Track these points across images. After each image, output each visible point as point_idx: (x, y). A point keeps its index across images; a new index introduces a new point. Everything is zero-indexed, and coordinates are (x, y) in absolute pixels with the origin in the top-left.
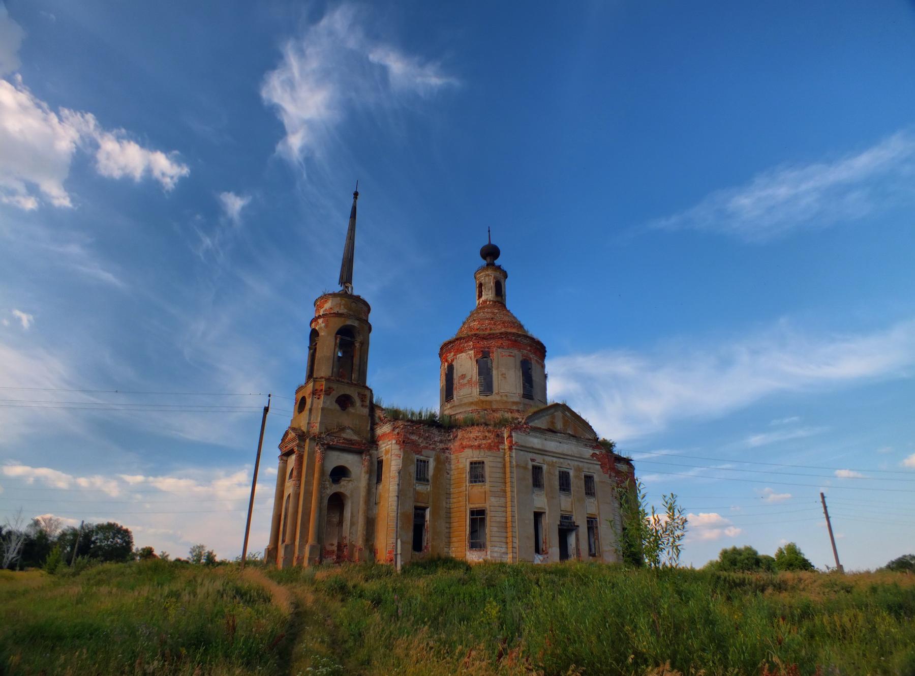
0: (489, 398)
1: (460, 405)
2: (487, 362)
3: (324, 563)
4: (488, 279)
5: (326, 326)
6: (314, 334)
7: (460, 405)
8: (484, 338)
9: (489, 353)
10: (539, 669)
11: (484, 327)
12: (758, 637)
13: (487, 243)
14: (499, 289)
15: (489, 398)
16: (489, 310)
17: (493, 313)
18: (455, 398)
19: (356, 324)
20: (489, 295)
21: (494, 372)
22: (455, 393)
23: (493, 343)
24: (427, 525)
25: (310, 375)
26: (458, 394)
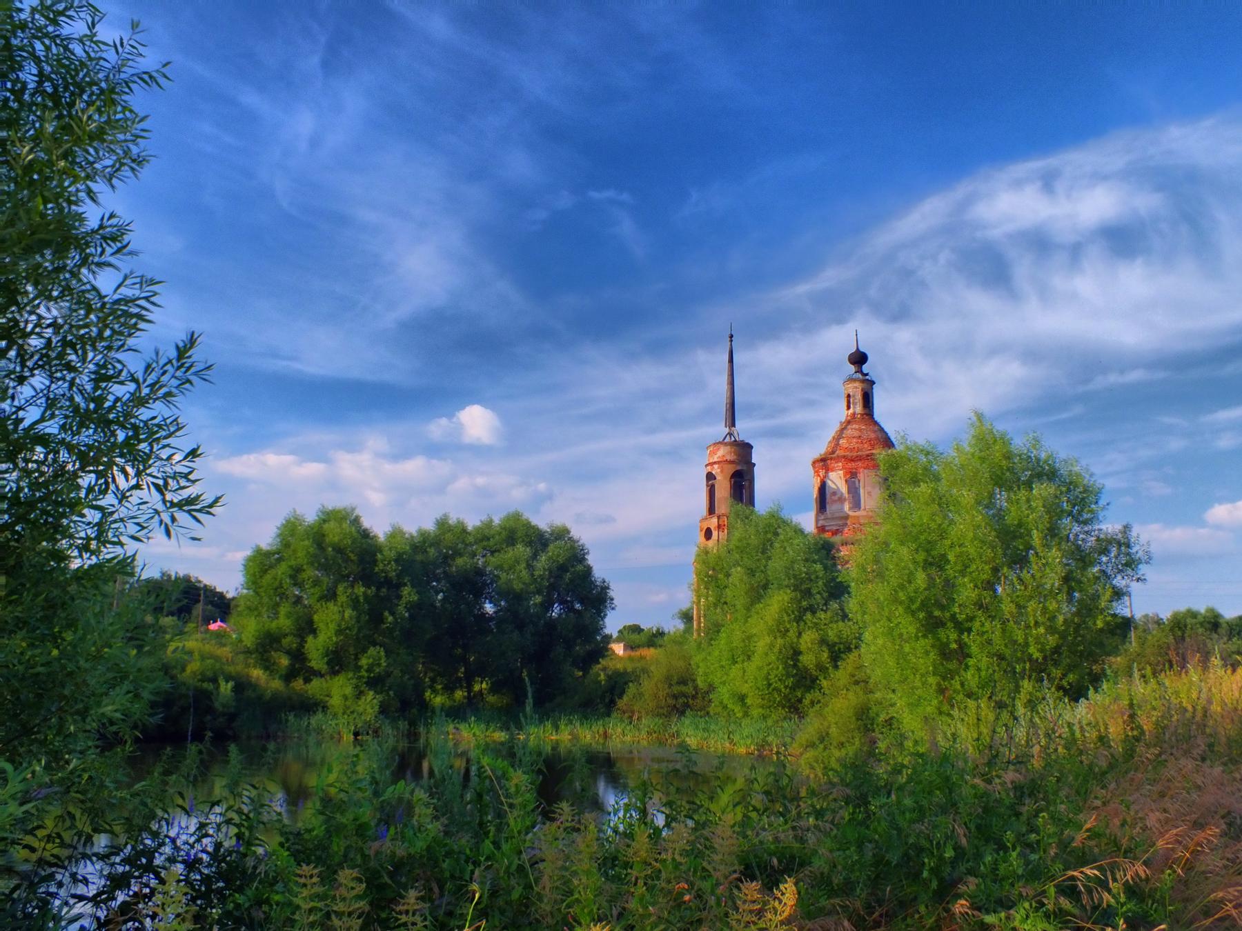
0: (857, 514)
1: (833, 519)
2: (854, 482)
3: (1226, 811)
4: (856, 390)
5: (722, 471)
6: (710, 477)
7: (833, 519)
8: (852, 460)
9: (856, 473)
10: (392, 570)
11: (852, 446)
12: (221, 884)
13: (854, 350)
14: (867, 400)
15: (857, 514)
16: (857, 427)
17: (860, 430)
18: (828, 512)
19: (745, 468)
20: (859, 409)
21: (862, 491)
22: (828, 506)
23: (860, 464)
24: (1084, 886)
25: (711, 510)
26: (831, 508)
